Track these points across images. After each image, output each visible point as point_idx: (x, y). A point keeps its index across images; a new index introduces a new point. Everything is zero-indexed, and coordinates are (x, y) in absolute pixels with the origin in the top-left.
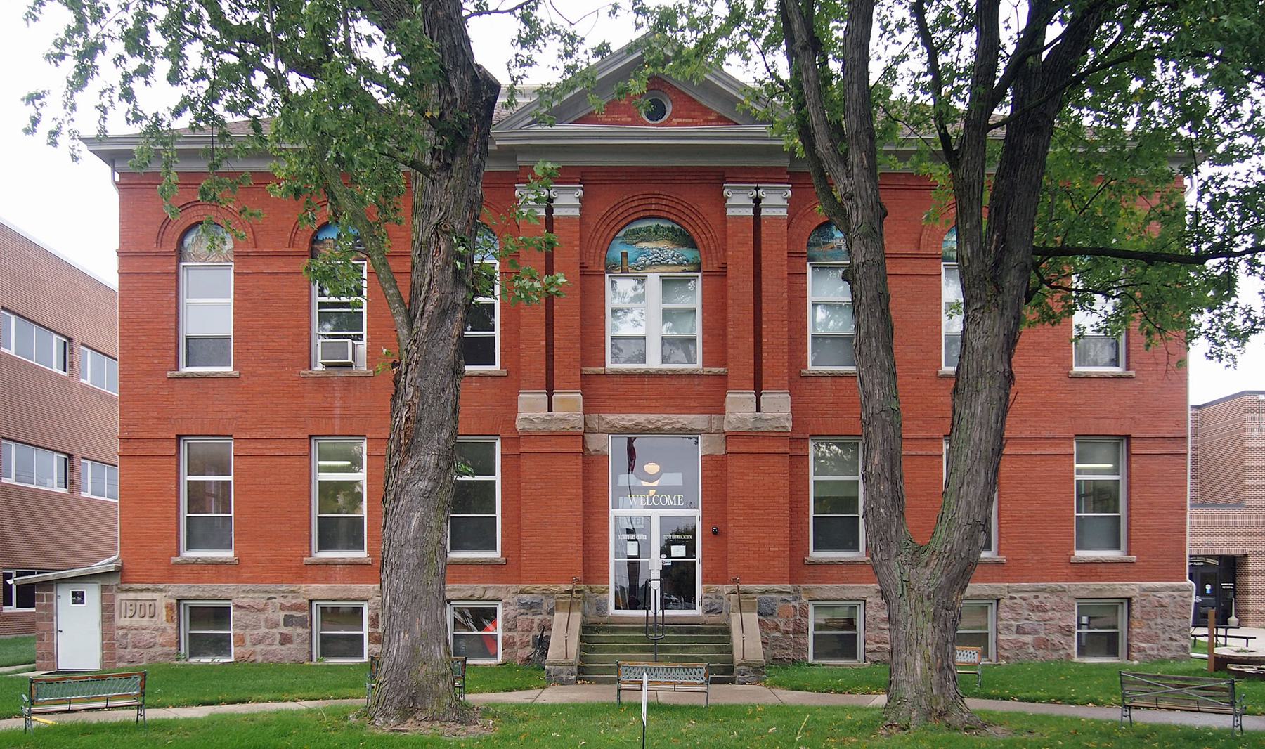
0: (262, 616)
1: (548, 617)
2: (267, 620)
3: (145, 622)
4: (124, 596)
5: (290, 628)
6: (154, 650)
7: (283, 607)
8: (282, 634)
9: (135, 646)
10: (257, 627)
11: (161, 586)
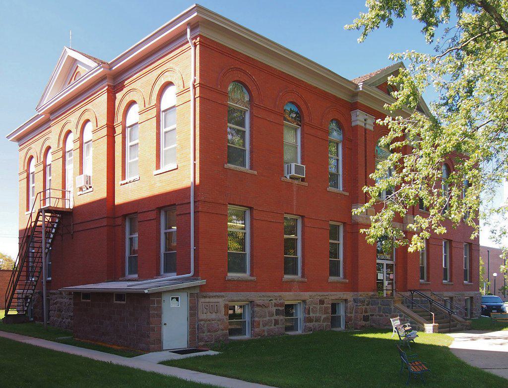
0: (266, 310)
1: (367, 307)
2: (269, 312)
3: (214, 316)
4: (203, 300)
5: (278, 316)
6: (219, 333)
7: (276, 305)
8: (275, 320)
9: (209, 331)
10: (265, 317)
11: (222, 294)
